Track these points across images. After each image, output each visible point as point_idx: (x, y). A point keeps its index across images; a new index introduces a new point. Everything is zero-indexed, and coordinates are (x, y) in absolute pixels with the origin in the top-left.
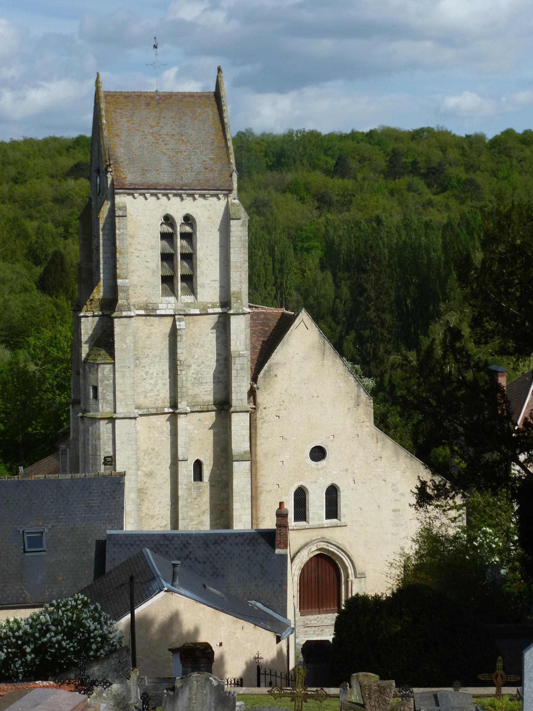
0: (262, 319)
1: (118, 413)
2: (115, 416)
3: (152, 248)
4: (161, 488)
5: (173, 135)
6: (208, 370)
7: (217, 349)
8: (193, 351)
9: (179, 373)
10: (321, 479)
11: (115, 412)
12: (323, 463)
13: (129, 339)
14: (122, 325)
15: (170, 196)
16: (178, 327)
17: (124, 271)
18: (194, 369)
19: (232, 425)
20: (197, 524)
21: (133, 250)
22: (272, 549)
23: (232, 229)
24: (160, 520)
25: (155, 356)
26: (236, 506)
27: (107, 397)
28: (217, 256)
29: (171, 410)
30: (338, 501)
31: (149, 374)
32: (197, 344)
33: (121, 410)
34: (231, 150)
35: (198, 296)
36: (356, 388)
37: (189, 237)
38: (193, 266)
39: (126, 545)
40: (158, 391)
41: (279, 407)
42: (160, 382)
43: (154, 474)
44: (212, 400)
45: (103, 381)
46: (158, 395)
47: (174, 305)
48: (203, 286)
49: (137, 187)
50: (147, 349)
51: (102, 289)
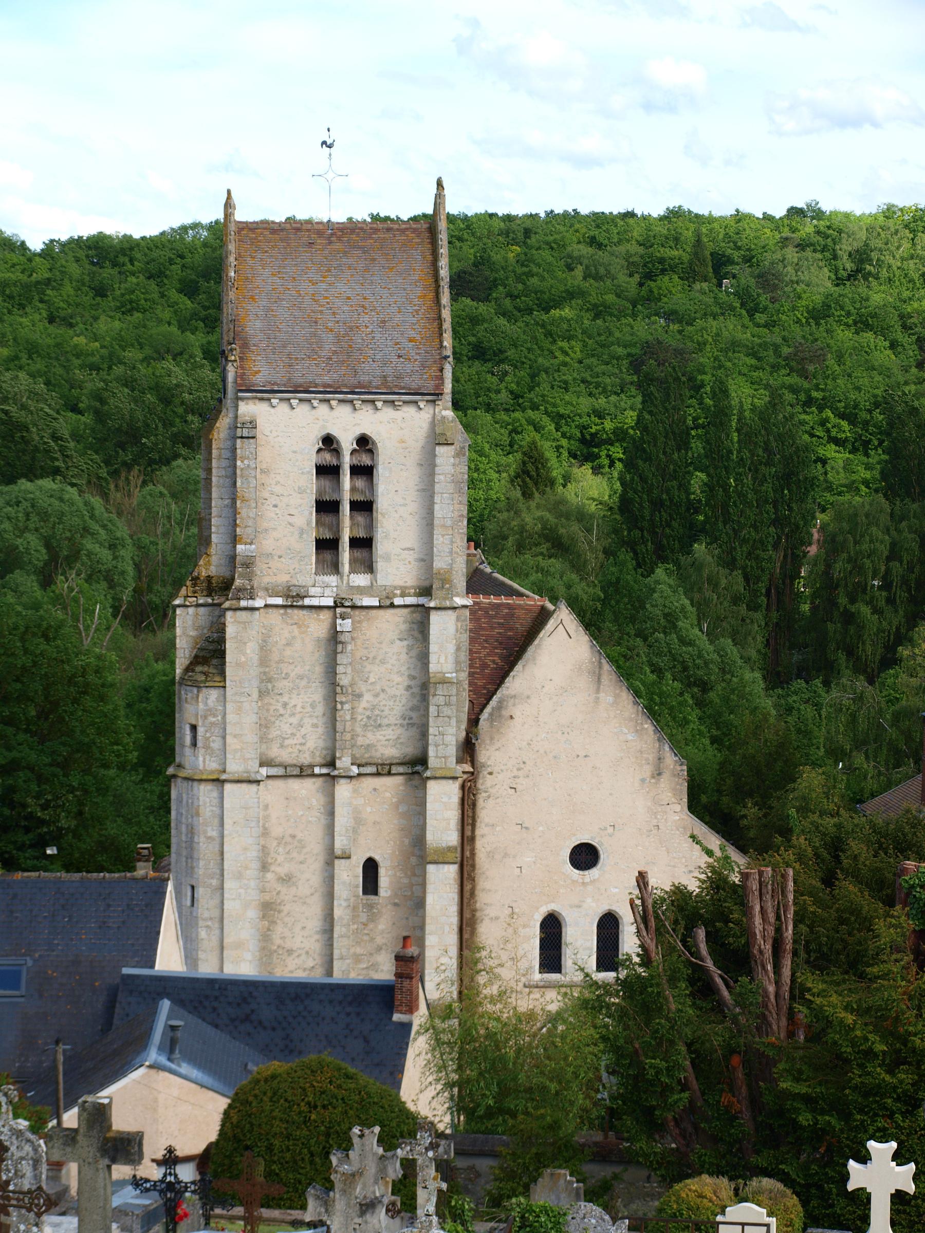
0: (504, 617)
1: (229, 774)
2: (224, 777)
3: (301, 491)
4: (305, 903)
5: (348, 298)
8: (367, 670)
9: (339, 706)
10: (589, 900)
12: (594, 873)
14: (239, 622)
17: (249, 530)
18: (368, 702)
19: (428, 800)
20: (367, 968)
21: (266, 494)
23: (438, 461)
24: (303, 957)
25: (301, 677)
27: (212, 745)
29: (325, 771)
30: (620, 940)
31: (288, 707)
32: (374, 658)
34: (447, 325)
35: (379, 576)
36: (657, 745)
37: (364, 472)
39: (150, 993)
41: (516, 773)
42: (308, 722)
43: (294, 880)
46: (304, 744)
47: (335, 589)
48: (387, 558)
49: (276, 388)
50: (286, 665)
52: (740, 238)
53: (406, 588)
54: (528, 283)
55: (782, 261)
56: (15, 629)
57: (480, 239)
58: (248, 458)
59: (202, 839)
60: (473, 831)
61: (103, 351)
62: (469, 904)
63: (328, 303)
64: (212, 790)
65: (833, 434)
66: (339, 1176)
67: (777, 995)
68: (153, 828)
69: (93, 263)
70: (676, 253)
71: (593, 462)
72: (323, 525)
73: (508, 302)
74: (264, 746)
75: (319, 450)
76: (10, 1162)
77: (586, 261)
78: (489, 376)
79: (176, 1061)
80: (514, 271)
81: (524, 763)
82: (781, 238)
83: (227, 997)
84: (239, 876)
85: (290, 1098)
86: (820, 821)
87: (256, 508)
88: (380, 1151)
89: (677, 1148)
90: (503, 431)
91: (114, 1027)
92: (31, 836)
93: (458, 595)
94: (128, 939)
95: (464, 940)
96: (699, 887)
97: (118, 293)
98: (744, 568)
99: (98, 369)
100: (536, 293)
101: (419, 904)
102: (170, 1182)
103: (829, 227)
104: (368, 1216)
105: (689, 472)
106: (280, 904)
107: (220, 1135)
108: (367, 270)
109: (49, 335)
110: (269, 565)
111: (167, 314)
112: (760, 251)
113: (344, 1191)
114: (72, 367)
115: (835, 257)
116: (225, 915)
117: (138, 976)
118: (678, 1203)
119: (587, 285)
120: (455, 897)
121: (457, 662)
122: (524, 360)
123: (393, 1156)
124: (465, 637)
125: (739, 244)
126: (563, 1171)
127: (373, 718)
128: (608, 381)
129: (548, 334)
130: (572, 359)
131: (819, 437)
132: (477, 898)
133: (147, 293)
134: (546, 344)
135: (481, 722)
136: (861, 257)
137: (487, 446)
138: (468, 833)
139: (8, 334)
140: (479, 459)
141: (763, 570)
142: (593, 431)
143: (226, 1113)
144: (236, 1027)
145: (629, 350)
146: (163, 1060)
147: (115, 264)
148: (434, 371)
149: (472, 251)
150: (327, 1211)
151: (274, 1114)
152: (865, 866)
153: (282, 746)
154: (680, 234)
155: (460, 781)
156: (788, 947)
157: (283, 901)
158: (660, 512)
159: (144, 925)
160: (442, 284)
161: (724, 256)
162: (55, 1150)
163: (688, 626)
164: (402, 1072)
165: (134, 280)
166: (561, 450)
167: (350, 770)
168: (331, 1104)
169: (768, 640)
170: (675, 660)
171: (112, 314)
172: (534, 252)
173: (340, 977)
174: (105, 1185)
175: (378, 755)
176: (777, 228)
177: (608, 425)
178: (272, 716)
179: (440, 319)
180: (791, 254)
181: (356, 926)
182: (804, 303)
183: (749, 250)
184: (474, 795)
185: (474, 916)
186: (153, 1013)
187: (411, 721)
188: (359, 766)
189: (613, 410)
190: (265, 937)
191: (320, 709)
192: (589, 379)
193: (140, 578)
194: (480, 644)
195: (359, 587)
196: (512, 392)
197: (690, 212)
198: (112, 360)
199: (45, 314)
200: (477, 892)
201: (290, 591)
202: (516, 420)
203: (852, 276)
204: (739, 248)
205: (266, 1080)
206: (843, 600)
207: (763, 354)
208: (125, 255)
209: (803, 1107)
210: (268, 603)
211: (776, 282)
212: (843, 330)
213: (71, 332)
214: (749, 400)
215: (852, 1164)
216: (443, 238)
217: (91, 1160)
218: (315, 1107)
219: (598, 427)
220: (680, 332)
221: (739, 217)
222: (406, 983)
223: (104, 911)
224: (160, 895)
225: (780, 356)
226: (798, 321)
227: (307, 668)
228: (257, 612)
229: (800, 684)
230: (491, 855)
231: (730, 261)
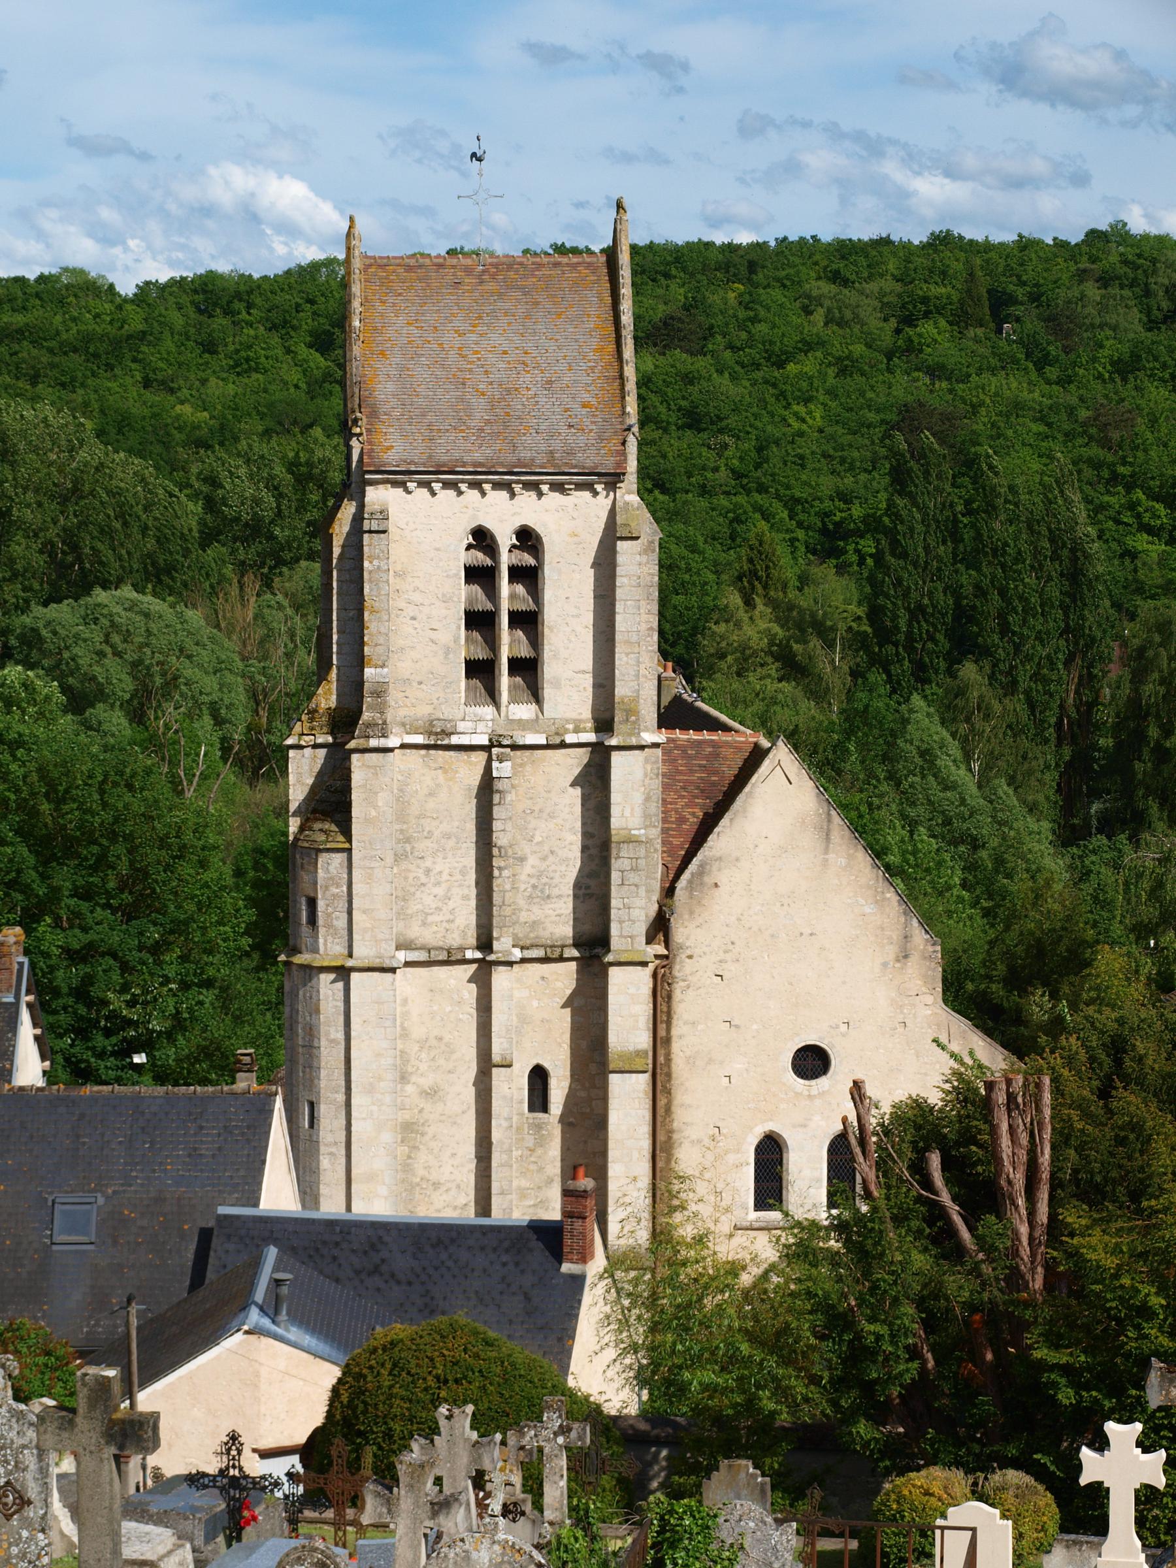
0: (707, 758)
2: (350, 963)
3: (446, 599)
5: (505, 353)
6: (563, 868)
7: (583, 824)
8: (531, 826)
9: (496, 873)
11: (350, 955)
13: (383, 799)
14: (369, 767)
15: (487, 487)
18: (533, 867)
19: (610, 991)
22: (556, 1264)
23: (620, 559)
24: (453, 1192)
25: (448, 836)
27: (335, 923)
28: (589, 618)
29: (478, 955)
31: (431, 874)
33: (364, 952)
34: (631, 386)
35: (546, 706)
36: (902, 919)
37: (528, 576)
38: (535, 640)
39: (253, 1238)
40: (452, 912)
41: (722, 956)
43: (441, 1093)
44: (571, 935)
45: (327, 888)
47: (490, 724)
48: (557, 685)
49: (413, 469)
50: (429, 820)
51: (334, 686)
52: (1025, 270)
53: (580, 721)
54: (753, 331)
55: (1081, 300)
56: (90, 777)
59: (323, 1043)
60: (668, 1030)
61: (212, 422)
63: (479, 359)
64: (333, 982)
65: (1146, 520)
66: (404, 1467)
67: (1031, 1238)
68: (269, 1029)
71: (838, 558)
73: (728, 354)
76: (9, 1451)
77: (827, 303)
79: (282, 1325)
80: (735, 316)
81: (733, 943)
82: (1078, 269)
83: (350, 1243)
85: (413, 1371)
87: (388, 621)
88: (474, 1435)
91: (207, 1281)
93: (647, 730)
94: (225, 1170)
95: (658, 1170)
96: (942, 1100)
97: (231, 348)
98: (1027, 693)
99: (208, 447)
100: (764, 344)
102: (234, 1476)
103: (1139, 256)
104: (441, 1518)
106: (423, 1124)
107: (327, 1418)
108: (528, 316)
110: (407, 694)
111: (294, 376)
112: (1050, 286)
114: (173, 444)
115: (1148, 293)
116: (353, 1139)
117: (238, 1217)
118: (898, 1503)
119: (830, 332)
120: (647, 1115)
121: (646, 816)
122: (749, 429)
123: (489, 1443)
124: (656, 784)
125: (1024, 278)
126: (744, 1462)
127: (540, 887)
128: (856, 454)
130: (810, 427)
132: (674, 1116)
135: (677, 891)
137: (701, 539)
138: (662, 1033)
139: (93, 402)
140: (691, 556)
142: (837, 519)
143: (335, 1391)
144: (362, 1281)
145: (882, 416)
146: (266, 1322)
147: (228, 312)
148: (614, 444)
149: (682, 291)
152: (1153, 1069)
153: (424, 924)
154: (948, 266)
155: (651, 966)
156: (1044, 1176)
157: (427, 1121)
158: (918, 623)
159: (246, 1152)
160: (624, 333)
161: (1004, 293)
162: (47, 1436)
165: (252, 332)
166: (797, 544)
167: (511, 953)
171: (225, 375)
172: (762, 291)
173: (501, 1217)
174: (111, 1479)
175: (546, 934)
176: (1073, 258)
177: (857, 511)
178: (411, 886)
179: (621, 377)
180: (1092, 291)
181: (520, 1152)
182: (1106, 352)
183: (1037, 285)
184: (669, 984)
185: (670, 1138)
186: (256, 1264)
187: (588, 891)
188: (522, 948)
189: (862, 491)
190: (406, 1167)
191: (472, 877)
192: (831, 452)
194: (676, 792)
195: (520, 720)
196: (733, 471)
197: (961, 238)
200: (673, 1109)
201: (433, 726)
203: (1170, 317)
204: (1024, 284)
205: (384, 1349)
207: (1053, 418)
208: (240, 300)
209: (1063, 1381)
210: (406, 741)
211: (1071, 326)
212: (1157, 388)
213: (172, 399)
214: (1037, 479)
215: (1086, 1453)
216: (625, 274)
217: (93, 1448)
218: (446, 1382)
219: (843, 515)
221: (1025, 245)
222: (578, 1224)
223: (195, 1134)
224: (266, 1114)
225: (1076, 421)
226: (1100, 376)
227: (456, 824)
228: (391, 754)
230: (690, 1060)
231: (1012, 300)
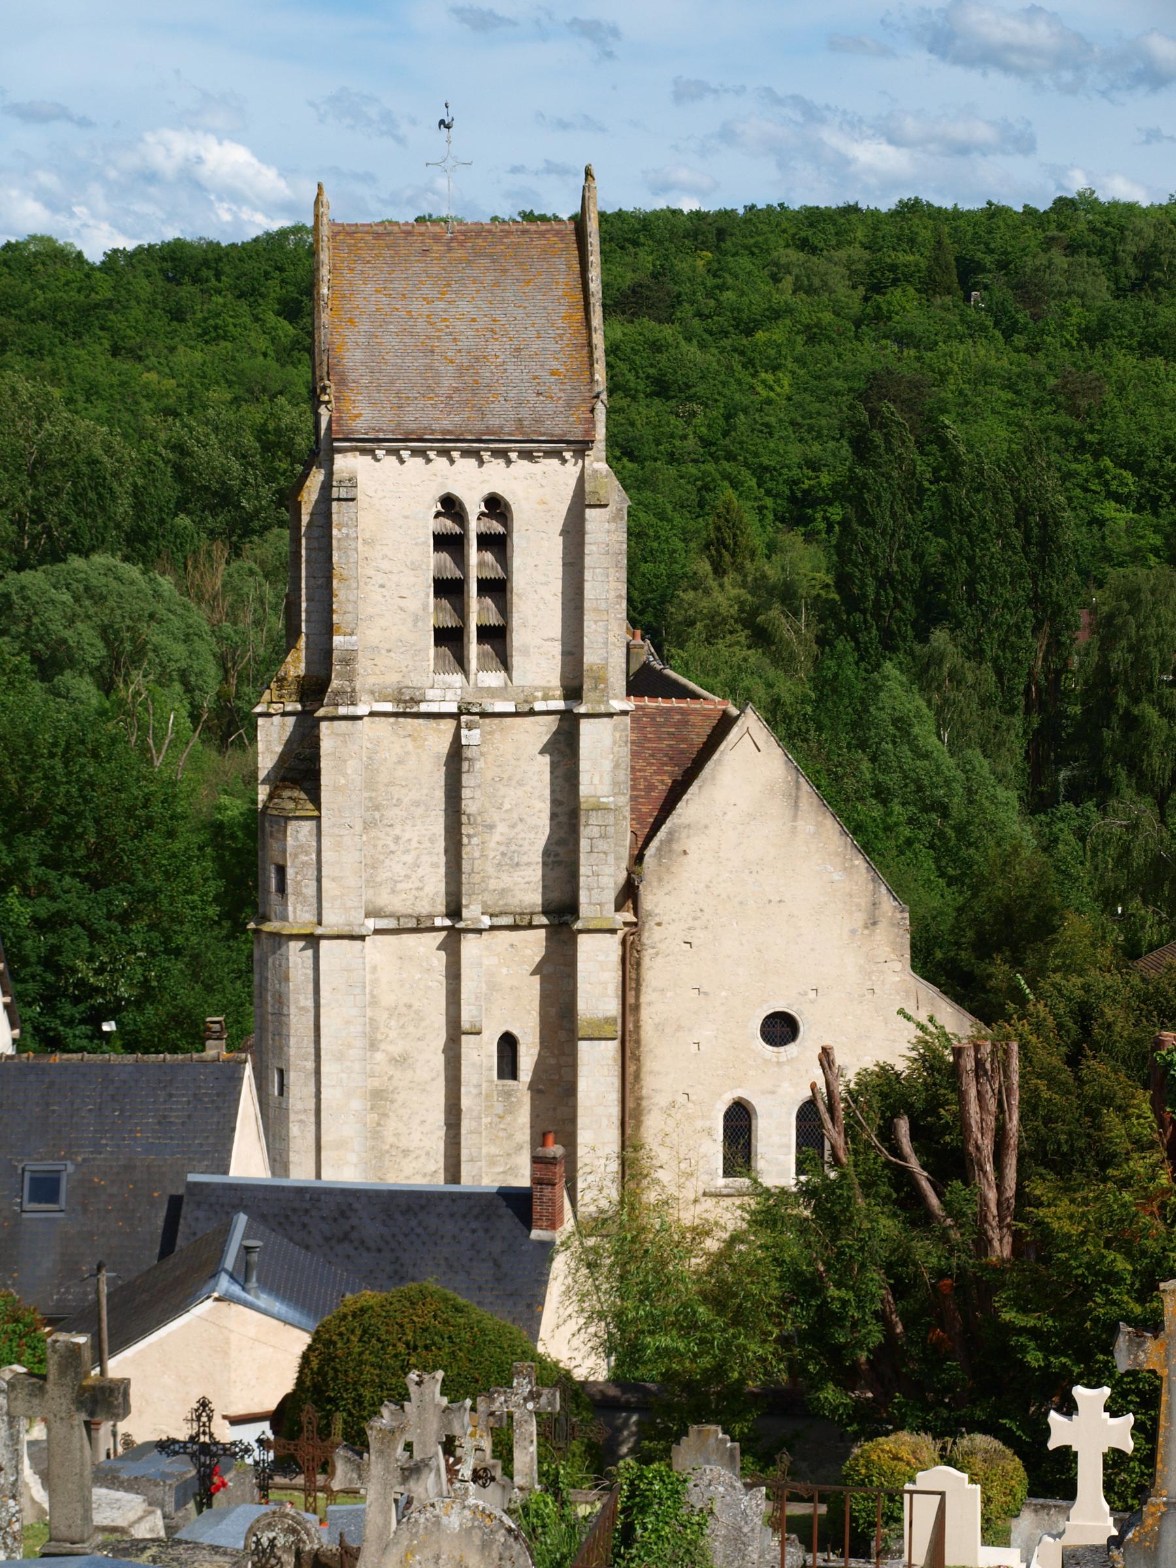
0: (676, 725)
2: (319, 931)
3: (414, 567)
5: (474, 320)
9: (465, 840)
10: (786, 1084)
11: (320, 923)
13: (352, 767)
15: (456, 454)
16: (464, 742)
23: (589, 527)
24: (423, 1159)
25: (417, 804)
26: (294, 1130)
27: (304, 890)
28: (557, 586)
29: (448, 922)
32: (510, 779)
33: (333, 919)
34: (599, 354)
35: (514, 674)
36: (871, 886)
37: (496, 544)
38: (504, 608)
40: (421, 879)
41: (691, 923)
43: (410, 1061)
45: (296, 856)
48: (526, 652)
49: (381, 436)
51: (303, 654)
57: (660, 242)
58: (347, 525)
60: (637, 997)
61: (180, 390)
62: (633, 1091)
64: (303, 949)
65: (1113, 488)
67: (999, 1204)
69: (168, 279)
70: (911, 258)
71: (806, 526)
72: (443, 609)
73: (696, 322)
74: (371, 892)
75: (438, 515)
77: (796, 271)
78: (672, 418)
84: (340, 1057)
86: (1063, 982)
88: (444, 1401)
89: (874, 1399)
90: (689, 487)
92: (82, 1007)
93: (615, 697)
97: (199, 316)
98: (995, 660)
99: (176, 414)
100: (732, 311)
101: (569, 1090)
103: (1107, 224)
105: (927, 539)
107: (297, 1384)
108: (496, 284)
109: (113, 371)
111: (263, 344)
113: (381, 1452)
115: (1115, 261)
117: (207, 1184)
120: (617, 1082)
121: (615, 783)
124: (625, 752)
125: (992, 246)
126: (713, 1427)
128: (824, 422)
129: (749, 364)
131: (1095, 492)
132: (643, 1083)
133: (237, 316)
134: (745, 376)
135: (647, 859)
136: (1148, 260)
137: (669, 508)
138: (631, 1000)
141: (1020, 662)
142: (806, 486)
143: (305, 1357)
146: (236, 1289)
147: (196, 280)
149: (650, 258)
150: (360, 1477)
151: (365, 1357)
153: (393, 891)
155: (620, 934)
160: (592, 300)
161: (972, 261)
162: (18, 1403)
163: (925, 733)
164: (543, 1305)
165: (221, 300)
168: (434, 1344)
169: (1027, 752)
170: (906, 777)
171: (192, 343)
175: (516, 902)
176: (1041, 225)
177: (825, 479)
179: (590, 344)
180: (1060, 260)
182: (1074, 320)
183: (1005, 253)
185: (639, 1105)
186: (225, 1232)
188: (491, 916)
189: (831, 459)
190: (376, 1134)
191: (441, 844)
192: (799, 420)
193: (226, 679)
194: (645, 759)
196: (701, 439)
197: (929, 205)
198: (193, 402)
199: (107, 344)
200: (642, 1075)
202: (705, 474)
204: (992, 251)
205: (354, 1315)
206: (1122, 700)
207: (1021, 386)
208: (209, 268)
213: (140, 367)
214: (1005, 446)
215: (1054, 1417)
216: (594, 241)
218: (415, 1348)
220: (919, 359)
222: (547, 1190)
226: (1068, 344)
227: (425, 791)
229: (1067, 807)
230: (659, 1028)
231: (980, 268)
